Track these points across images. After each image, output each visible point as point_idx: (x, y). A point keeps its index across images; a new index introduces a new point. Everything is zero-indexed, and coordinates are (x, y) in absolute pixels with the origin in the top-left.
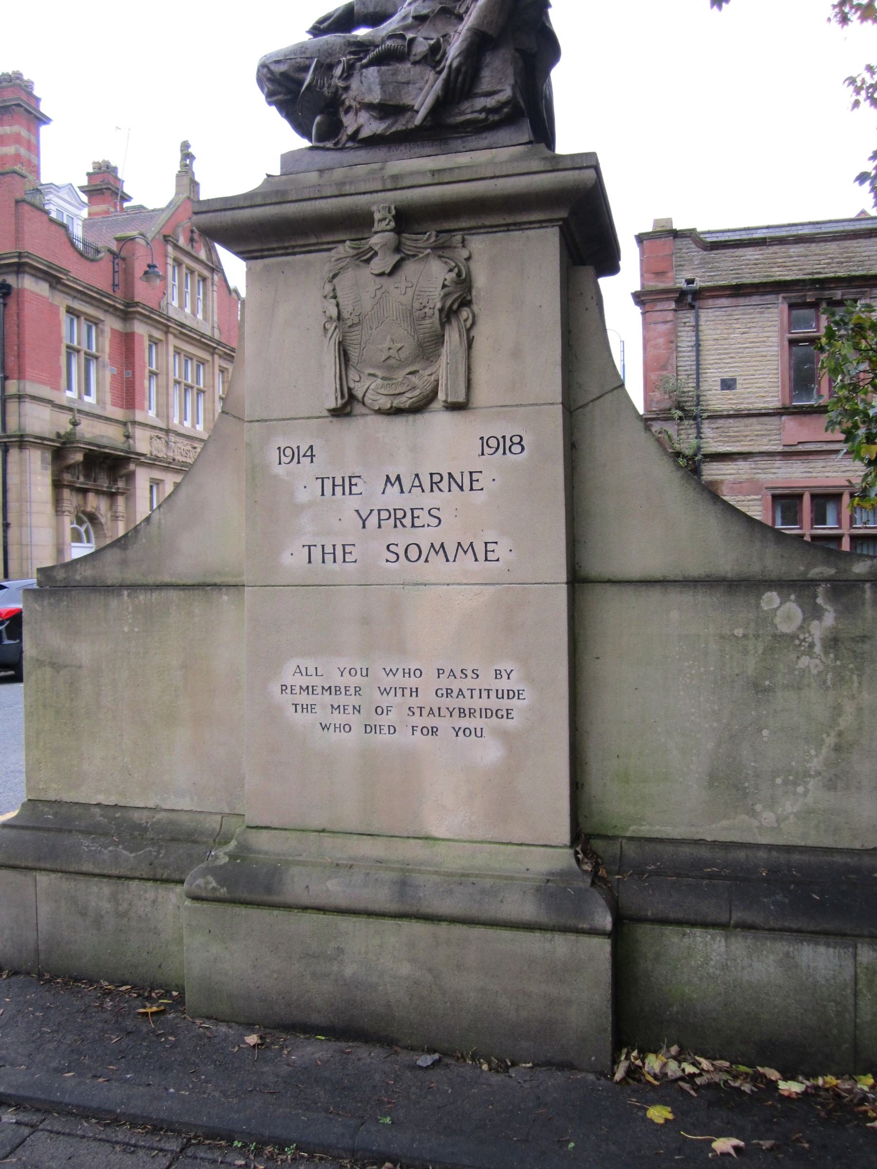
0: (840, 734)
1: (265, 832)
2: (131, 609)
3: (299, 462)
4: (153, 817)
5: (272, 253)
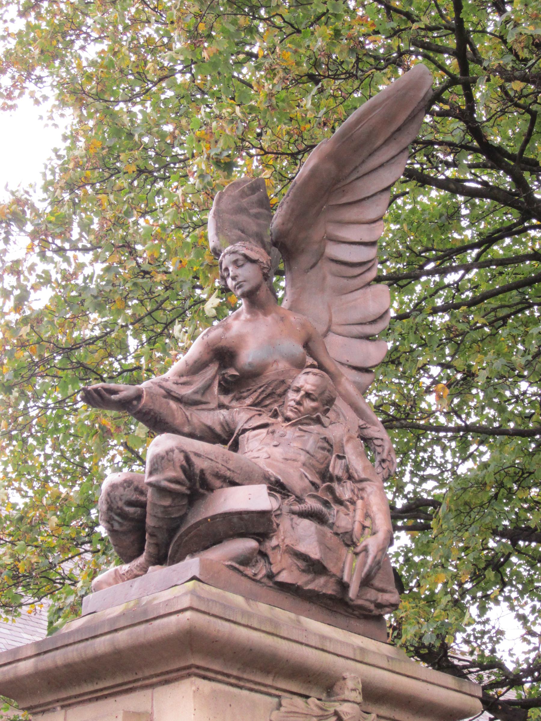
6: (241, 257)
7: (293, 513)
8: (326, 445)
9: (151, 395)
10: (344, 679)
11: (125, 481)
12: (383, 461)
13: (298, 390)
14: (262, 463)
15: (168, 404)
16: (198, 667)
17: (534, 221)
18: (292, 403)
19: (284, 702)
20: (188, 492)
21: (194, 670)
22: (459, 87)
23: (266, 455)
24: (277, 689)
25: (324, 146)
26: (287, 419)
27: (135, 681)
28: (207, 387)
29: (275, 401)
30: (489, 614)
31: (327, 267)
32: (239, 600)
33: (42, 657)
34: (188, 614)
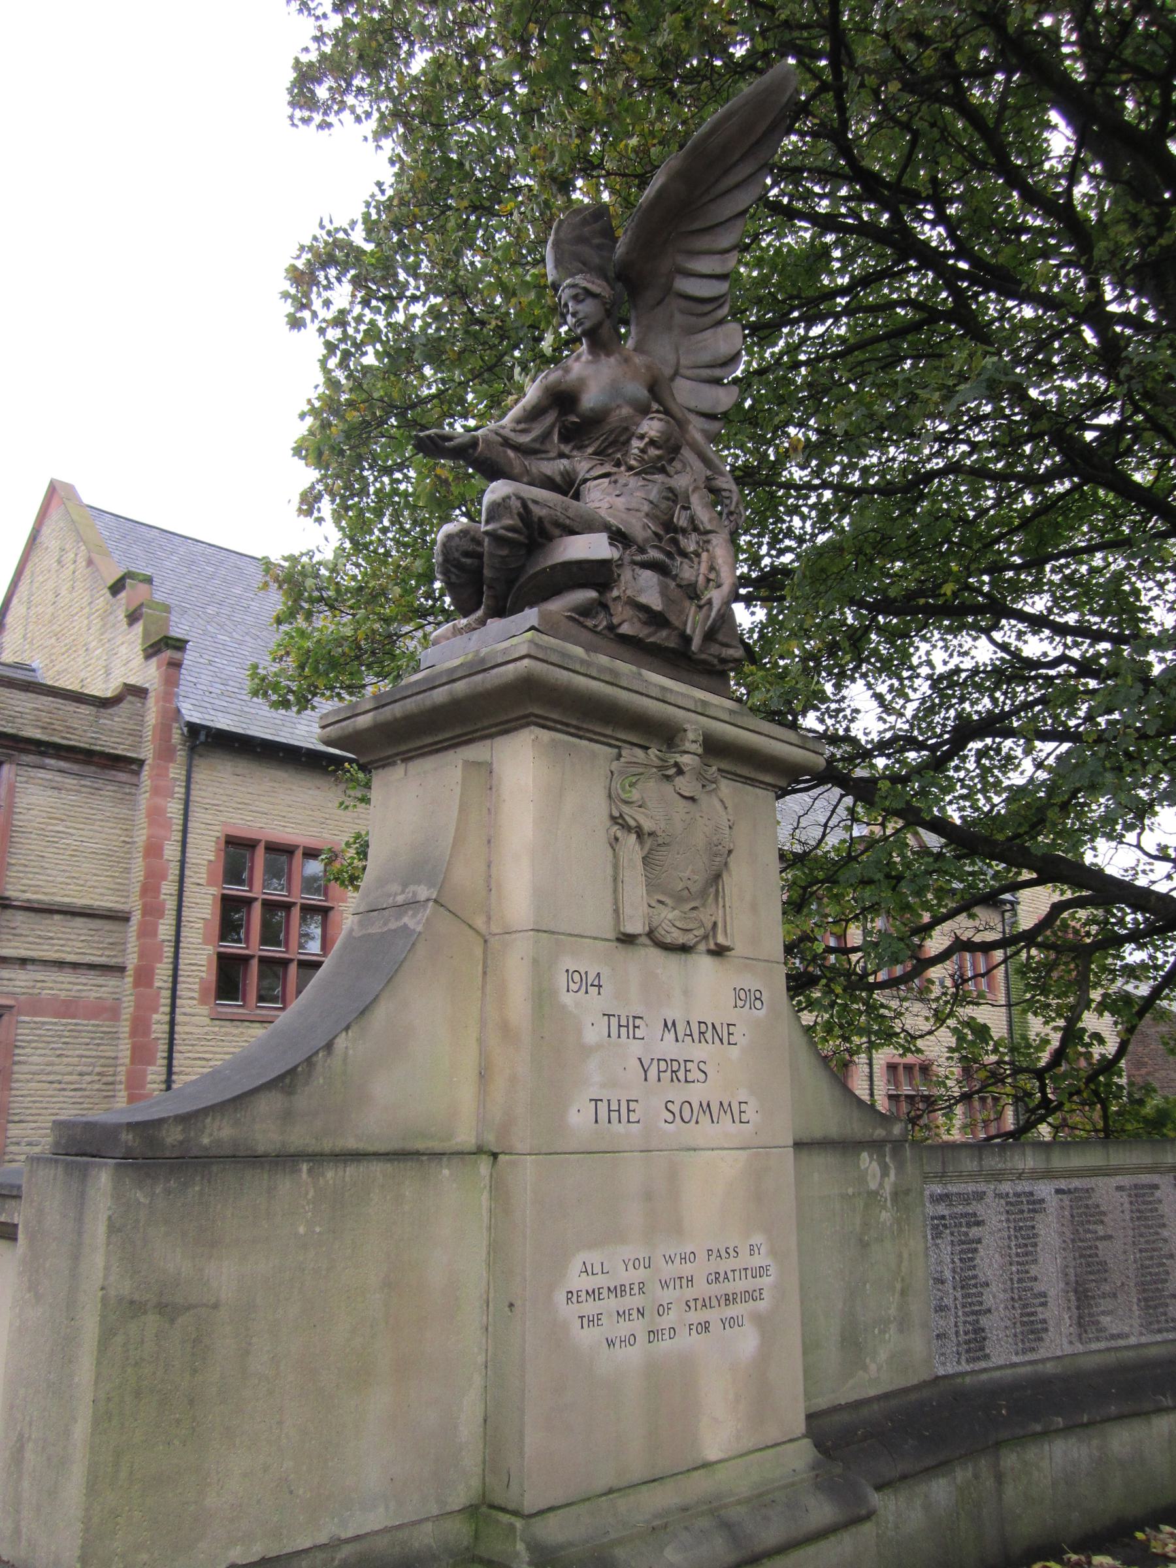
0: (903, 1280)
1: (551, 1515)
2: (311, 1194)
3: (587, 992)
4: (333, 1559)
5: (565, 728)
6: (580, 291)
7: (634, 563)
8: (670, 495)
9: (486, 441)
10: (685, 730)
11: (461, 531)
12: (731, 513)
13: (642, 437)
14: (603, 513)
15: (505, 452)
16: (537, 716)
17: (913, 263)
18: (636, 451)
19: (624, 753)
20: (526, 541)
21: (533, 719)
22: (830, 96)
23: (607, 505)
24: (617, 739)
25: (672, 162)
26: (630, 468)
27: (476, 731)
28: (545, 436)
29: (618, 450)
30: (845, 692)
31: (676, 304)
32: (579, 651)
33: (380, 710)
34: (526, 662)
